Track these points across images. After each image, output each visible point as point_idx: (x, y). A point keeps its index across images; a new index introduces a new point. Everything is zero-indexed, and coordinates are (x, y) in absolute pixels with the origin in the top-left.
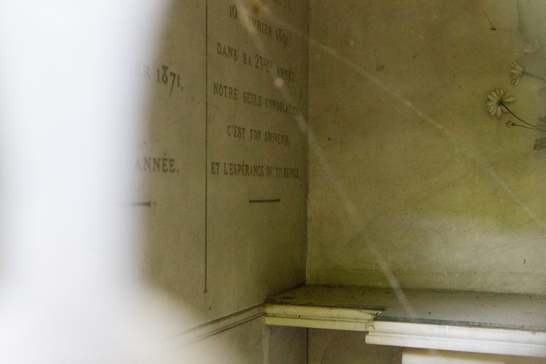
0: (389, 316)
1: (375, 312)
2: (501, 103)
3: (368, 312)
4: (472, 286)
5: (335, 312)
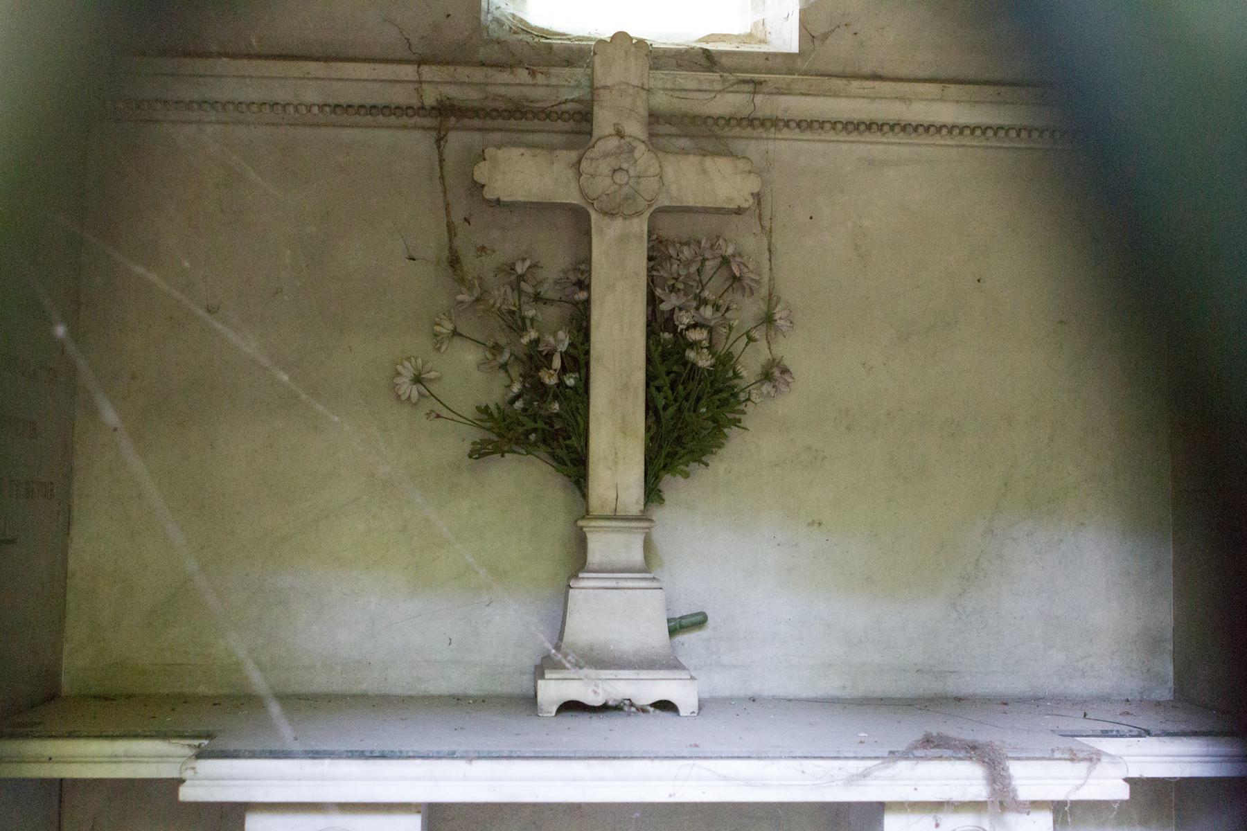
0: (225, 748)
1: (196, 742)
2: (418, 380)
3: (183, 742)
4: (363, 687)
5: (121, 746)
